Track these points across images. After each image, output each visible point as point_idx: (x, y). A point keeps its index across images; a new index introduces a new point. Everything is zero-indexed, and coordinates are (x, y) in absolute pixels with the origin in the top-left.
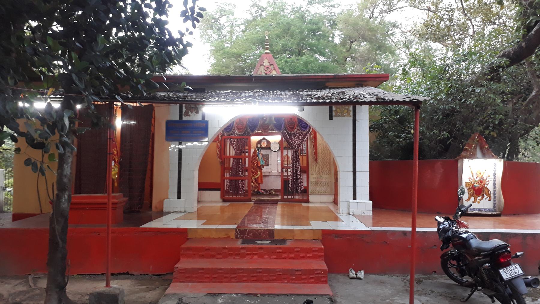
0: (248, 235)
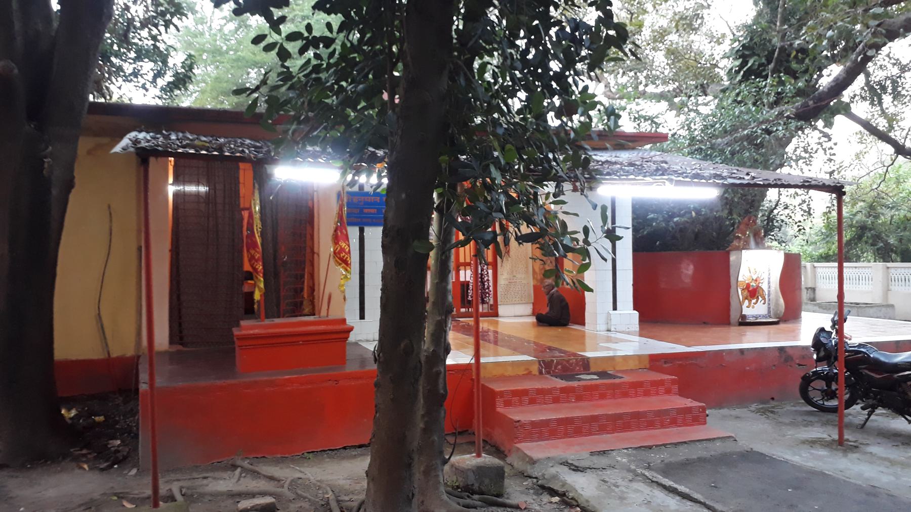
0: (556, 368)
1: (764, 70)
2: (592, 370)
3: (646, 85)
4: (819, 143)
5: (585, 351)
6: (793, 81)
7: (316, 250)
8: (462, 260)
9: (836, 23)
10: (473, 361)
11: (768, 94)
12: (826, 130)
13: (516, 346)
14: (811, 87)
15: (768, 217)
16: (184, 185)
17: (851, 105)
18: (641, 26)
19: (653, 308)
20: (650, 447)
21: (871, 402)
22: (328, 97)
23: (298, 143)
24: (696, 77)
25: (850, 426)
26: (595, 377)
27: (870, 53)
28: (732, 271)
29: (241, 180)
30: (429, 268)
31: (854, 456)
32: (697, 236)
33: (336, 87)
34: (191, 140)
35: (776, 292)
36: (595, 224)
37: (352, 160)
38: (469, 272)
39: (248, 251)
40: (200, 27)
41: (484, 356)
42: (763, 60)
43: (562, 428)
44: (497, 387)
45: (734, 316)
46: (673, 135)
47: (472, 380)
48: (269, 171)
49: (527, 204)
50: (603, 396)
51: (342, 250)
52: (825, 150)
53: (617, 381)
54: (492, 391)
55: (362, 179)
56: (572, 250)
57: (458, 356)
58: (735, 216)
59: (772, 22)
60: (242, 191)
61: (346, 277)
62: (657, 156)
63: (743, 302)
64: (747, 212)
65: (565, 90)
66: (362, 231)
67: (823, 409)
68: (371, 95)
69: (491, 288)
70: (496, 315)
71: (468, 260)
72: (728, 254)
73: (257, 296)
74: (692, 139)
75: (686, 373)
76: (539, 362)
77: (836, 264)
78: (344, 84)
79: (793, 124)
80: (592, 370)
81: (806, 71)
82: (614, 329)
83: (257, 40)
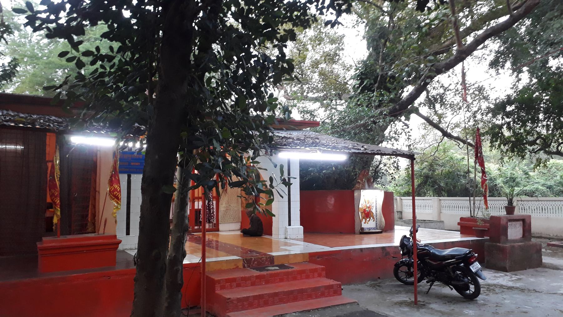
1: (373, 87)
2: (276, 264)
3: (308, 93)
4: (404, 130)
5: (271, 252)
6: (388, 94)
7: (97, 189)
8: (196, 195)
9: (410, 63)
10: (201, 261)
11: (375, 101)
12: (406, 122)
13: (229, 250)
14: (398, 98)
15: (375, 170)
16: (6, 145)
17: (419, 108)
18: (304, 58)
19: (312, 225)
20: (309, 311)
21: (431, 278)
22: (109, 93)
23: (87, 122)
24: (335, 89)
25: (420, 293)
26: (277, 268)
27: (428, 81)
28: (355, 202)
29: (47, 143)
30: (174, 200)
31: (422, 310)
32: (336, 181)
33: (114, 86)
34: (13, 116)
35: (380, 214)
36: (277, 176)
37: (123, 133)
38: (201, 203)
39: (50, 190)
40: (23, 40)
41: (209, 257)
42: (372, 82)
43: (256, 302)
44: (216, 278)
45: (357, 229)
46: (322, 122)
47: (200, 273)
48: (66, 138)
49: (236, 163)
50: (282, 280)
51: (115, 190)
52: (405, 133)
53: (290, 270)
54: (213, 280)
55: (130, 144)
56: (263, 192)
57: (191, 259)
58: (357, 170)
59: (376, 60)
60: (48, 149)
61: (117, 207)
62: (313, 134)
63: (362, 220)
64: (364, 168)
65: (260, 96)
66: (129, 177)
67: (407, 283)
68: (138, 91)
69: (215, 213)
70: (218, 230)
71: (200, 195)
72: (353, 193)
73: (55, 220)
74: (333, 125)
75: (329, 264)
76: (243, 260)
77: (411, 198)
78: (121, 85)
79: (388, 119)
80: (276, 264)
81: (395, 89)
82: (289, 238)
83: (63, 54)
